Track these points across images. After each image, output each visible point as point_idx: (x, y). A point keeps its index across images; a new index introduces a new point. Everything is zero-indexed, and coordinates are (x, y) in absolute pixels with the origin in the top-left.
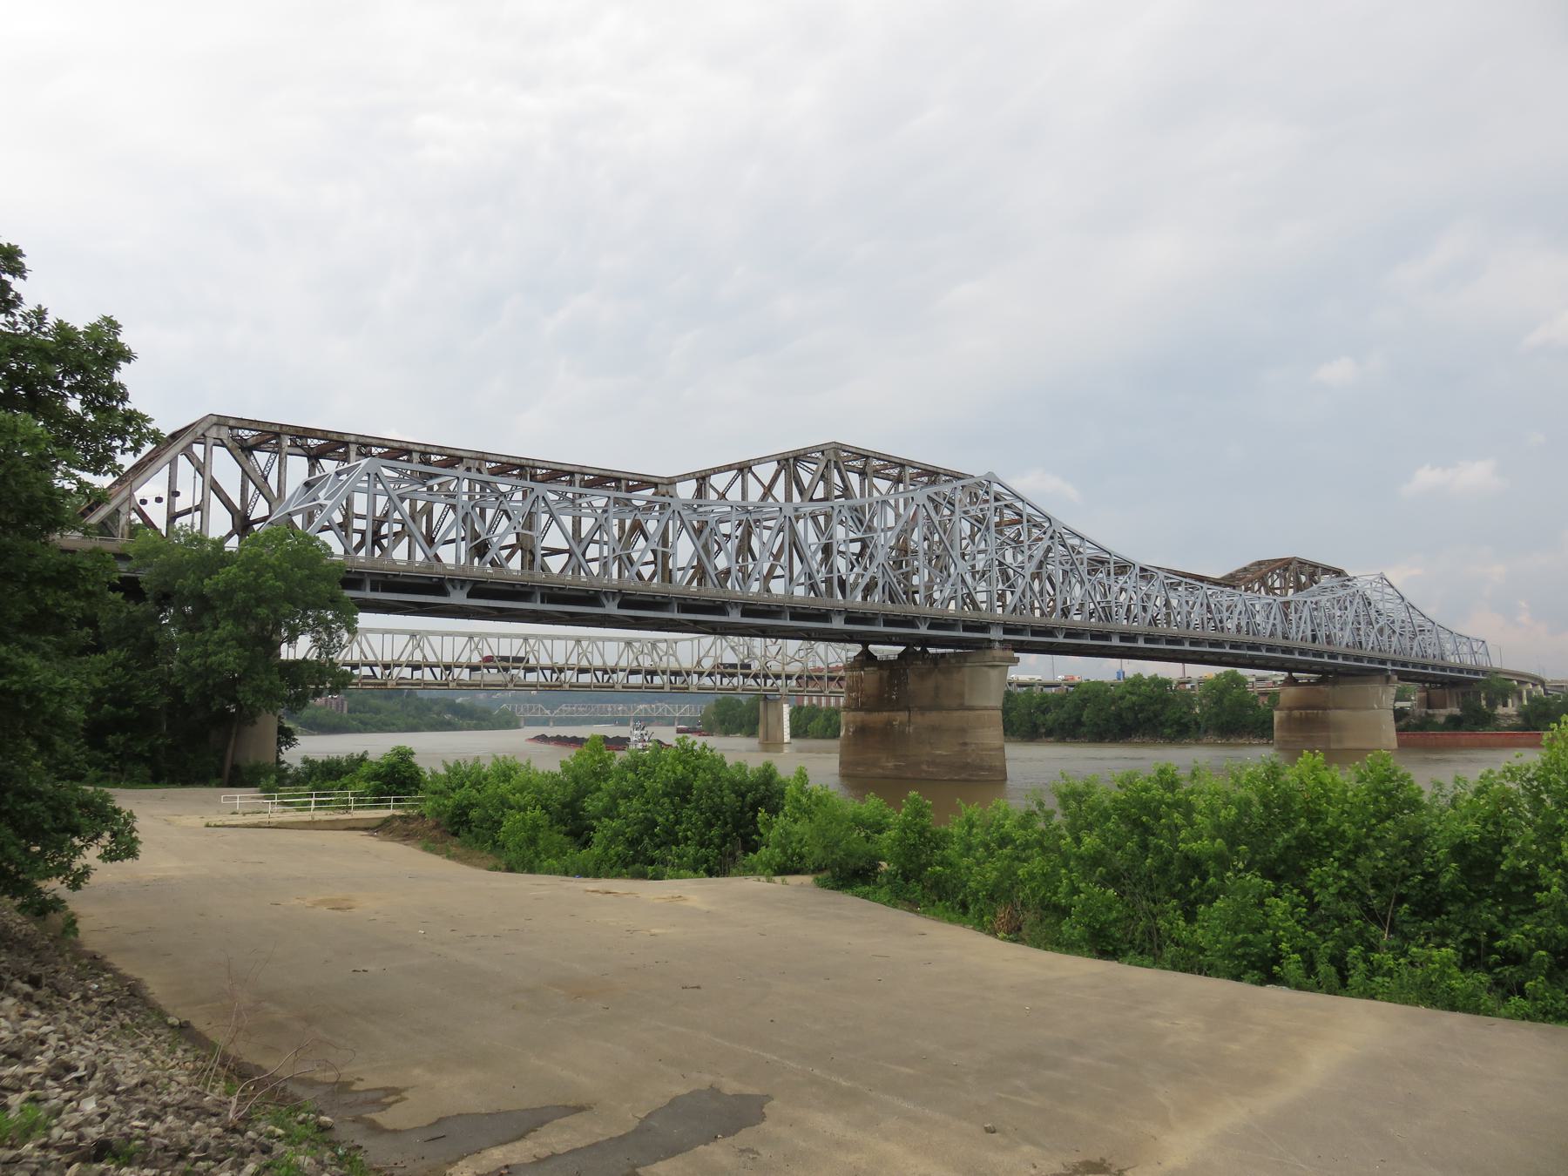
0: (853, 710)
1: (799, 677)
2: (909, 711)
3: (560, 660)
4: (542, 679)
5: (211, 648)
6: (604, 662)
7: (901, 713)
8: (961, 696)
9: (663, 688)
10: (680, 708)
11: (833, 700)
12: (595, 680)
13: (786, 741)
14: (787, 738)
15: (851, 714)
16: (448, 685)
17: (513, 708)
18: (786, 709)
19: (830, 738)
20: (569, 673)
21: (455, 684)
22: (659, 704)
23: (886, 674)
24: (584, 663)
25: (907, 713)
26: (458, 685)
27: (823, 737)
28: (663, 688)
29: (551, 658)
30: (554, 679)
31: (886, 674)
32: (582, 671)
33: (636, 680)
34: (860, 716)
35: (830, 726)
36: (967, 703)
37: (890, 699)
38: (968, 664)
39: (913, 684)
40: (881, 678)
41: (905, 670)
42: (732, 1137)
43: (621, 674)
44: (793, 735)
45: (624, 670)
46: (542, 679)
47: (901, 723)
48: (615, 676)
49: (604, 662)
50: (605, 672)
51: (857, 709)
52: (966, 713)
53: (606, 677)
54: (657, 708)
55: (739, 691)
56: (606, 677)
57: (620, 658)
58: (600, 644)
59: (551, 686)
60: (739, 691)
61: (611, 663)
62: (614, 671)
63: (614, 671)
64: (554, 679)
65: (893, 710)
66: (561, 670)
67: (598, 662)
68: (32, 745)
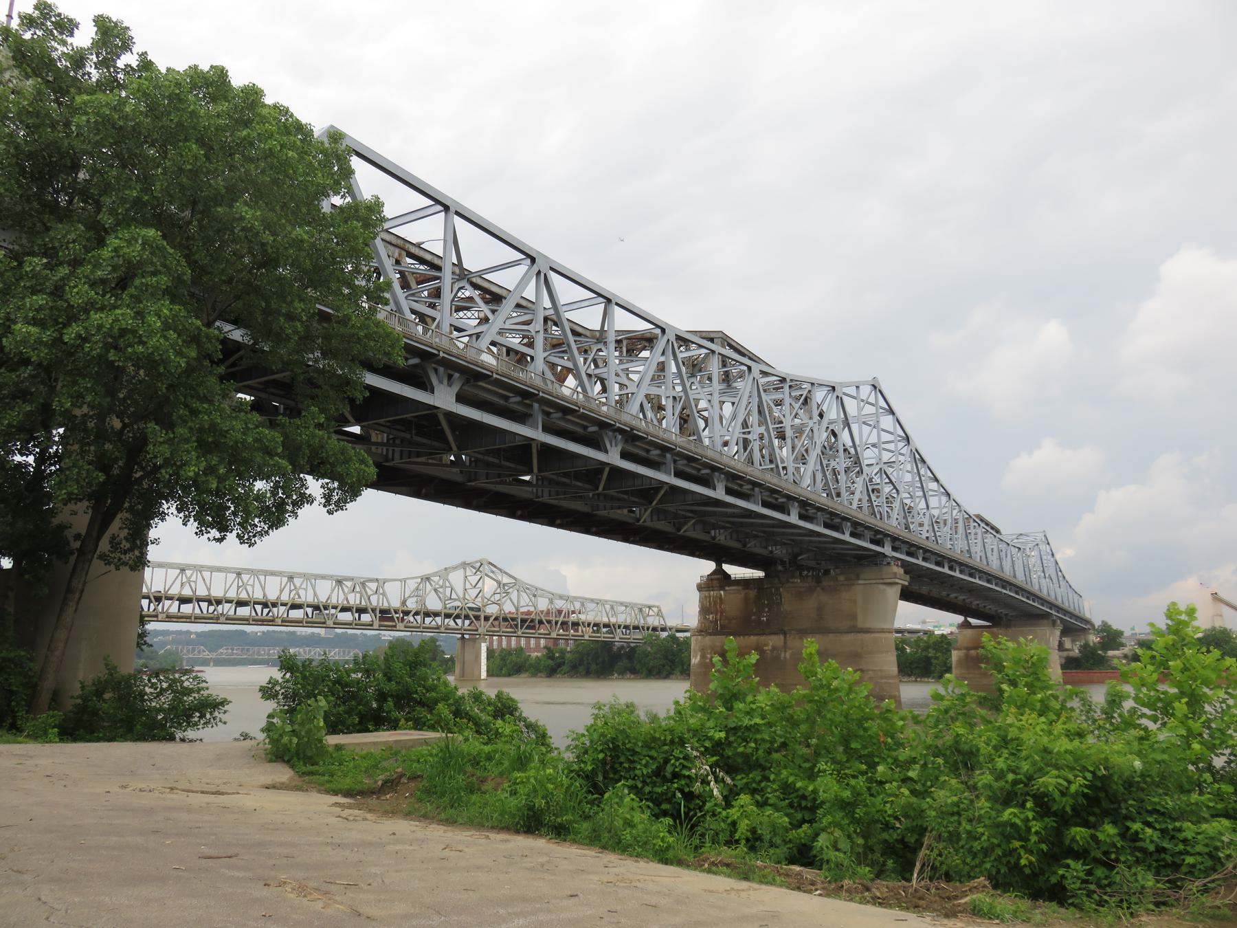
0: (710, 634)
1: (496, 619)
2: (785, 634)
3: (217, 592)
4: (197, 611)
5: (79, 293)
6: (265, 595)
7: (774, 638)
8: (854, 617)
9: (372, 625)
10: (349, 652)
11: (523, 641)
12: (254, 614)
13: (482, 677)
14: (484, 675)
15: (708, 638)
16: (156, 616)
17: (177, 649)
18: (484, 647)
19: (504, 676)
20: (227, 606)
21: (164, 616)
22: (307, 649)
23: (753, 593)
24: (244, 596)
25: (782, 637)
26: (167, 617)
27: (498, 676)
28: (372, 625)
29: (209, 590)
30: (265, 614)
31: (753, 593)
32: (241, 603)
33: (346, 617)
34: (708, 640)
35: (505, 665)
36: (860, 624)
37: (759, 622)
38: (860, 582)
39: (788, 603)
40: (746, 599)
41: (777, 589)
42: (1025, 904)
43: (282, 609)
44: (490, 673)
45: (285, 605)
46: (197, 611)
47: (774, 648)
48: (275, 610)
49: (265, 595)
50: (265, 605)
51: (715, 633)
52: (860, 636)
53: (266, 611)
54: (310, 651)
55: (442, 629)
56: (266, 611)
57: (281, 591)
58: (207, 574)
59: (263, 621)
60: (442, 629)
61: (272, 597)
62: (274, 605)
63: (274, 605)
64: (265, 614)
65: (763, 634)
66: (219, 602)
67: (258, 595)
68: (956, 598)
